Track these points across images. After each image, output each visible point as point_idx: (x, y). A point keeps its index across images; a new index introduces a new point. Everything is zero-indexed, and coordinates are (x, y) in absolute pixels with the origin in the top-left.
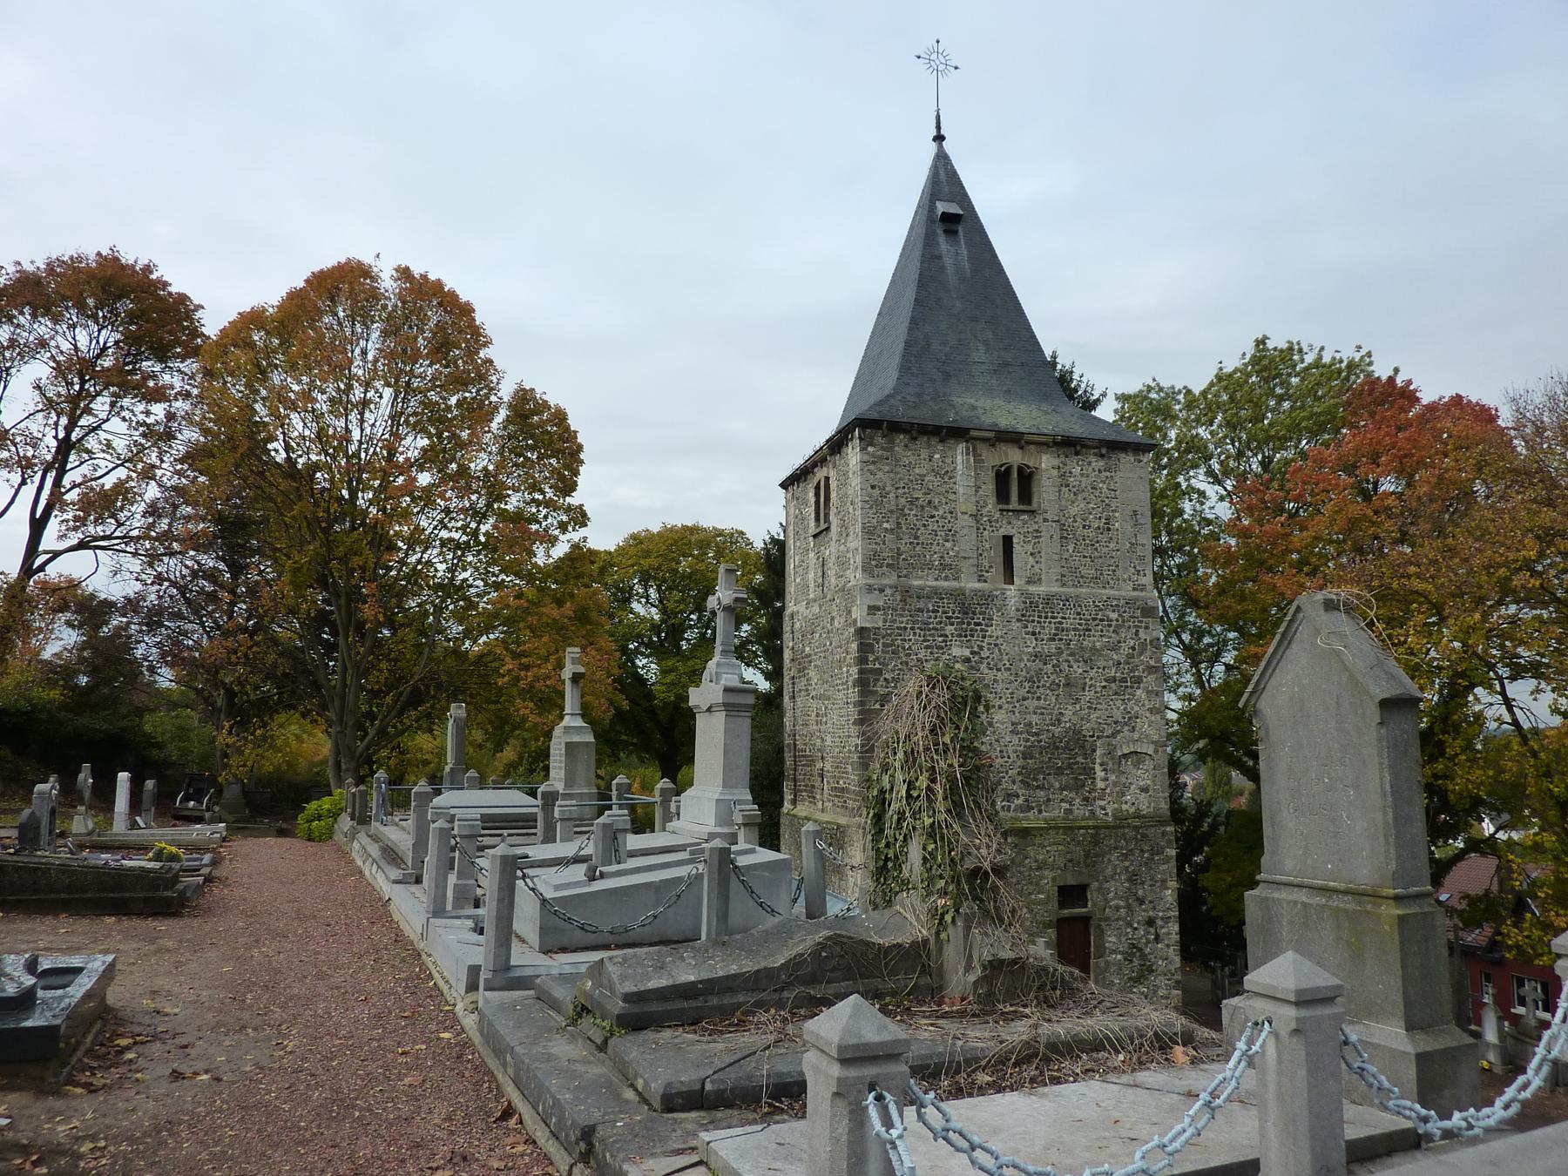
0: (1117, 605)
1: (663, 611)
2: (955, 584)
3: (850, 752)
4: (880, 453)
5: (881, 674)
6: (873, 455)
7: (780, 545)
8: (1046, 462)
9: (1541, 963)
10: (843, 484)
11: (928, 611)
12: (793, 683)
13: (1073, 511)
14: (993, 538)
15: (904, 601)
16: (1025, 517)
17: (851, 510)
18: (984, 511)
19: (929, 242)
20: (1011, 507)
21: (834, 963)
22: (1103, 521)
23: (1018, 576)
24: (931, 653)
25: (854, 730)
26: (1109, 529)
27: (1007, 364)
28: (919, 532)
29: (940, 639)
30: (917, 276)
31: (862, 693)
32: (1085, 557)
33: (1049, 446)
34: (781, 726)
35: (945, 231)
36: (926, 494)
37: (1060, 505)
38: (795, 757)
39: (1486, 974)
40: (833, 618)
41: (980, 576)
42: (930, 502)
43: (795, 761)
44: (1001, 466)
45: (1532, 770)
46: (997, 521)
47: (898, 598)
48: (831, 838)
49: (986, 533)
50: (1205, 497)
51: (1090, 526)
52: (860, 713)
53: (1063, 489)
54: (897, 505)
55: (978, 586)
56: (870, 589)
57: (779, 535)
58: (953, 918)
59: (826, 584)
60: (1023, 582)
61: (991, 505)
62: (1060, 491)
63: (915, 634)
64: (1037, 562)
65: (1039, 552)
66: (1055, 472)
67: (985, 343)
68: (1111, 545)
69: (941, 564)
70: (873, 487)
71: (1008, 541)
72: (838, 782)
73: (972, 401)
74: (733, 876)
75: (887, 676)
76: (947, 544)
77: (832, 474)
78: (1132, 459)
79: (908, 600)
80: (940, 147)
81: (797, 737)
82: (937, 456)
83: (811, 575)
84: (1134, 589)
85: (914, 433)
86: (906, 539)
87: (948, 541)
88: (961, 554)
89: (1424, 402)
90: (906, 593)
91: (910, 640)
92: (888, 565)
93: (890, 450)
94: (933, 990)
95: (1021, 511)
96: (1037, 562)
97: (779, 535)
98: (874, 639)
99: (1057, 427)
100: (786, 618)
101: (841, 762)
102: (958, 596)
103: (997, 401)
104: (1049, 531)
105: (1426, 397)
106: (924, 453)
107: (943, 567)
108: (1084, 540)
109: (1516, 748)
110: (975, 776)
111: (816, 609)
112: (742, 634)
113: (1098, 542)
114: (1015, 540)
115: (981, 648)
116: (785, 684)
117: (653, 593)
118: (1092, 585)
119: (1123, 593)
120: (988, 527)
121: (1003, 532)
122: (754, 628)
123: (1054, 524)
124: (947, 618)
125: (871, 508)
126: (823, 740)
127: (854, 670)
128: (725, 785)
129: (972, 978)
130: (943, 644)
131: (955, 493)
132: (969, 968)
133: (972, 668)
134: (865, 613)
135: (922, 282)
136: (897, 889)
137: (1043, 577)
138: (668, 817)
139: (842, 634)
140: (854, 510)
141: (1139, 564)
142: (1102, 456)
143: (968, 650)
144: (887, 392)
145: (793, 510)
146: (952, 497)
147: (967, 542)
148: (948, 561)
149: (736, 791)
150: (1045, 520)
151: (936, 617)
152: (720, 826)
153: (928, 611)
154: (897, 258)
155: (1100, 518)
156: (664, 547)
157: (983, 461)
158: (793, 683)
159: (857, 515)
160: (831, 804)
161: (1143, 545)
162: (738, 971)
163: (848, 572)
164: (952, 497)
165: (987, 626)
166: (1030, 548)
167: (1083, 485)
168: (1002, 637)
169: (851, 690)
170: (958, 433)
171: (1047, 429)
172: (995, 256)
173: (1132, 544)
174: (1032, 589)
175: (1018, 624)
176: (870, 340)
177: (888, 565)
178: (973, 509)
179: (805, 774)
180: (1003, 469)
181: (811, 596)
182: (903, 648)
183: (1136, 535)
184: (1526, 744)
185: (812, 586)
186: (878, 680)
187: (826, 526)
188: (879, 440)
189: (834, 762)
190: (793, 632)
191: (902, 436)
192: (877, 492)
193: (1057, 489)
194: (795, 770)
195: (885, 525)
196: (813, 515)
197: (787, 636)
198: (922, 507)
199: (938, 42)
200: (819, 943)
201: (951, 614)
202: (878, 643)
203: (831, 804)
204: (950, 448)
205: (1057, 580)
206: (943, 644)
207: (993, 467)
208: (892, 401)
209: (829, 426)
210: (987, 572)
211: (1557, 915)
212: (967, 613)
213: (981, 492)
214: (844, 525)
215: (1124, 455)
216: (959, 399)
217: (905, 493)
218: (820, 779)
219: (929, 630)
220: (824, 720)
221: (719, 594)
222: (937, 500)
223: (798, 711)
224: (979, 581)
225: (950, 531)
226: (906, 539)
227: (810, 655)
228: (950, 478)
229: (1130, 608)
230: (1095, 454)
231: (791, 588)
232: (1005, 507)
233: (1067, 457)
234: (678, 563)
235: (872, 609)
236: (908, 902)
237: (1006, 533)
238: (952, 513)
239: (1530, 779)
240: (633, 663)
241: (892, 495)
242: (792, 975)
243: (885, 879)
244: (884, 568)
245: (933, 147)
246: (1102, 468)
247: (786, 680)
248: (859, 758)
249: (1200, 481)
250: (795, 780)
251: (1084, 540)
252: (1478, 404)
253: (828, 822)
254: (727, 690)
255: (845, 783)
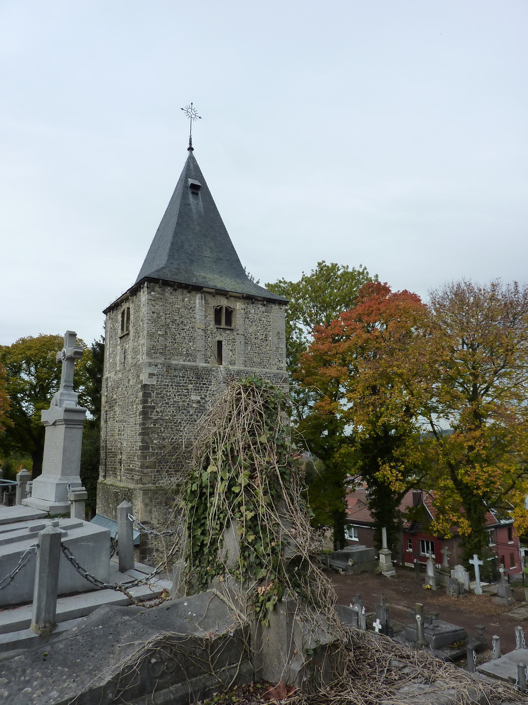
0: (270, 377)
1: (37, 377)
2: (194, 364)
3: (136, 450)
4: (157, 296)
5: (154, 408)
6: (154, 296)
7: (102, 347)
8: (239, 306)
9: (447, 538)
10: (137, 311)
11: (180, 377)
12: (106, 414)
13: (251, 330)
14: (212, 341)
15: (167, 371)
16: (228, 332)
17: (141, 324)
18: (209, 328)
19: (184, 196)
20: (222, 327)
21: (163, 668)
22: (264, 336)
23: (224, 361)
24: (181, 398)
25: (139, 438)
26: (267, 340)
27: (221, 259)
28: (177, 337)
29: (186, 391)
30: (178, 212)
31: (144, 419)
32: (255, 353)
33: (240, 299)
34: (99, 437)
35: (193, 193)
36: (180, 318)
37: (245, 327)
38: (106, 452)
39: (409, 540)
40: (129, 380)
41: (206, 360)
42: (182, 322)
43: (106, 455)
44: (218, 307)
45: (441, 452)
46: (215, 333)
47: (165, 370)
48: (125, 495)
49: (209, 339)
50: (302, 332)
51: (258, 338)
52: (143, 429)
53: (246, 319)
54: (166, 323)
55: (205, 365)
56: (150, 364)
57: (100, 341)
58: (275, 606)
59: (126, 362)
60: (227, 364)
61: (212, 325)
62: (245, 320)
63: (173, 388)
64: (233, 354)
65: (235, 350)
66: (243, 311)
67: (210, 248)
68: (268, 348)
69: (187, 353)
70: (153, 313)
71: (220, 343)
72: (129, 466)
73: (204, 275)
74: (62, 555)
75: (158, 410)
76: (190, 343)
77: (131, 306)
78: (278, 307)
79: (170, 371)
80: (191, 153)
81: (108, 442)
82: (186, 299)
83: (118, 358)
84: (277, 369)
85: (176, 287)
86: (170, 340)
87: (190, 342)
88: (197, 349)
89: (393, 292)
90: (169, 367)
91: (170, 391)
92: (160, 353)
93: (163, 294)
94: (254, 674)
95: (227, 329)
96: (233, 354)
97: (100, 341)
98: (152, 390)
99: (244, 290)
100: (104, 381)
101: (131, 455)
102: (194, 369)
103: (215, 276)
104: (240, 339)
105: (394, 290)
106: (180, 297)
107: (188, 355)
108: (255, 345)
109: (434, 443)
110: (288, 472)
111: (120, 375)
112: (79, 391)
113: (261, 346)
114: (223, 343)
115: (206, 396)
116: (102, 414)
117: (33, 369)
118: (258, 366)
119: (273, 371)
120: (210, 336)
121: (217, 339)
122: (86, 388)
123: (242, 336)
124: (189, 380)
125: (152, 323)
126: (122, 444)
127: (140, 407)
128: (63, 473)
129: (296, 667)
130: (187, 394)
131: (195, 318)
132: (293, 655)
133: (201, 406)
134: (147, 377)
135: (181, 215)
136: (214, 572)
137: (236, 361)
138: (24, 495)
139: (134, 388)
140: (143, 324)
141: (280, 357)
142: (264, 305)
143: (199, 397)
144: (161, 266)
145: (109, 324)
146: (193, 320)
147: (200, 344)
148: (190, 352)
149: (71, 477)
150: (238, 334)
151: (184, 380)
152: (59, 501)
153: (180, 377)
154: (168, 204)
155: (263, 335)
156: (40, 345)
157: (209, 304)
158: (106, 414)
159: (145, 327)
160: (125, 477)
161: (282, 348)
162: (60, 700)
163: (139, 356)
164: (193, 320)
165: (209, 385)
166: (230, 347)
167: (255, 319)
168: (216, 391)
169: (138, 417)
170: (197, 289)
171: (239, 290)
172: (216, 207)
173: (277, 348)
174: (231, 367)
175: (224, 385)
176: (153, 242)
177: (160, 353)
178: (203, 327)
179: (111, 462)
180: (218, 308)
181: (118, 369)
182: (167, 395)
183: (279, 343)
184: (438, 441)
185: (118, 363)
186: (153, 412)
187: (127, 332)
188: (157, 289)
189: (128, 455)
190: (107, 388)
191: (169, 288)
192: (155, 315)
193: (243, 319)
194: (106, 459)
195: (159, 332)
196: (120, 327)
197: (104, 389)
198: (178, 324)
199: (192, 104)
200: (149, 650)
201: (191, 379)
202: (153, 392)
203: (125, 477)
204: (193, 296)
205: (243, 363)
206: (187, 394)
207: (214, 307)
208: (165, 270)
209: (131, 281)
210: (209, 358)
211: (453, 516)
212: (199, 379)
213: (207, 319)
214: (137, 332)
215: (274, 305)
216: (198, 273)
217: (170, 317)
218: (119, 464)
219: (180, 386)
220: (123, 433)
221: (64, 349)
222: (185, 322)
223: (108, 429)
224: (205, 362)
225: (192, 337)
226: (170, 340)
227: (115, 399)
228: (193, 311)
229: (275, 378)
230: (261, 304)
231: (107, 365)
232: (219, 327)
233: (248, 304)
234: (47, 353)
235: (151, 375)
236: (225, 586)
237: (219, 340)
238: (193, 328)
239: (440, 456)
240: (20, 405)
241: (163, 317)
242: (119, 691)
243: (200, 562)
244: (158, 354)
245: (187, 153)
246: (264, 311)
247: (103, 412)
248: (142, 453)
249: (300, 325)
250: (106, 465)
251: (255, 345)
252: (413, 294)
253: (123, 487)
254: (67, 411)
255: (133, 466)
